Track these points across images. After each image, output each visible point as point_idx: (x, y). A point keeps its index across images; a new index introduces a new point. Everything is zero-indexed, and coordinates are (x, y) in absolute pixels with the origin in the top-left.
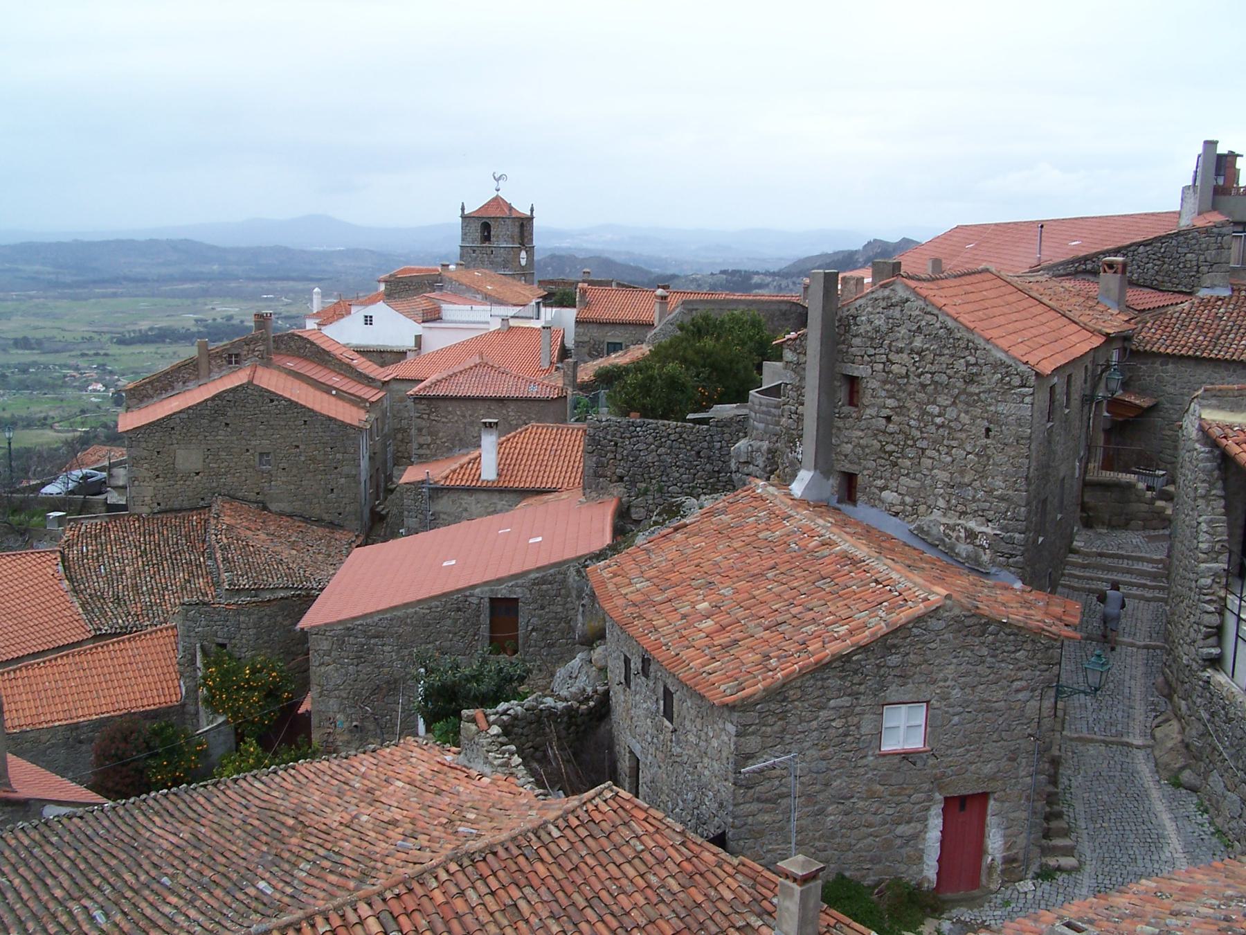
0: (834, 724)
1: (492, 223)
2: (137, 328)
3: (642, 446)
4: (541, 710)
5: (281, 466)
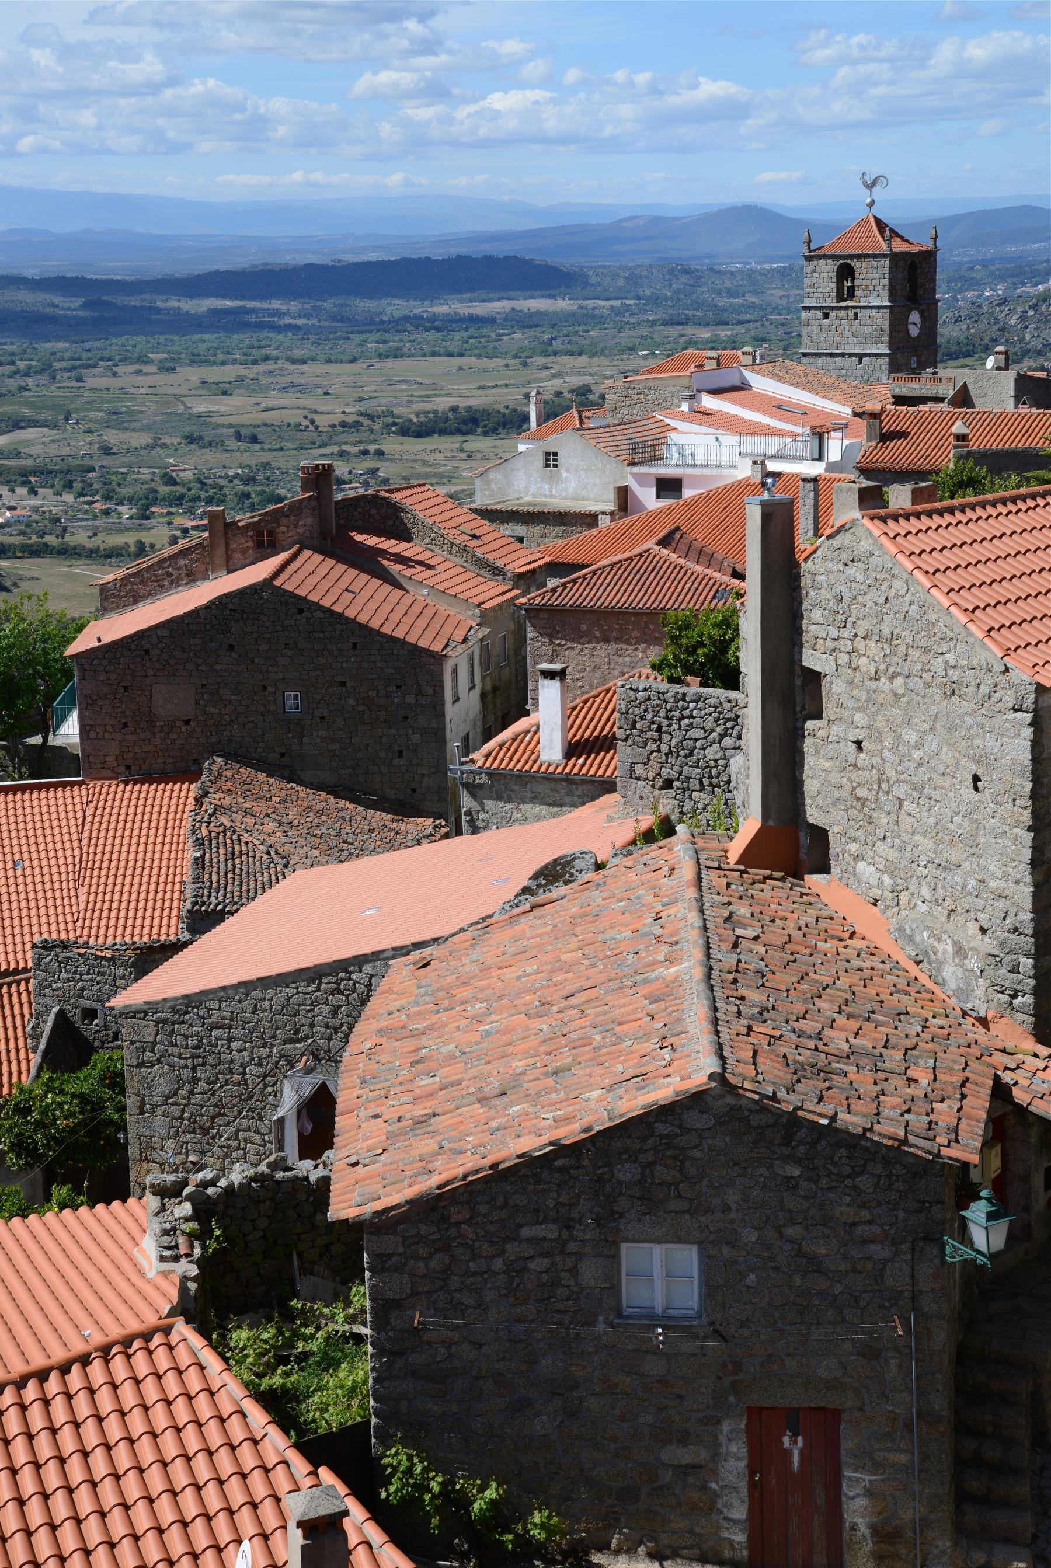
0: (532, 1265)
1: (856, 264)
2: (429, 407)
3: (697, 733)
4: (278, 1183)
5: (318, 713)
